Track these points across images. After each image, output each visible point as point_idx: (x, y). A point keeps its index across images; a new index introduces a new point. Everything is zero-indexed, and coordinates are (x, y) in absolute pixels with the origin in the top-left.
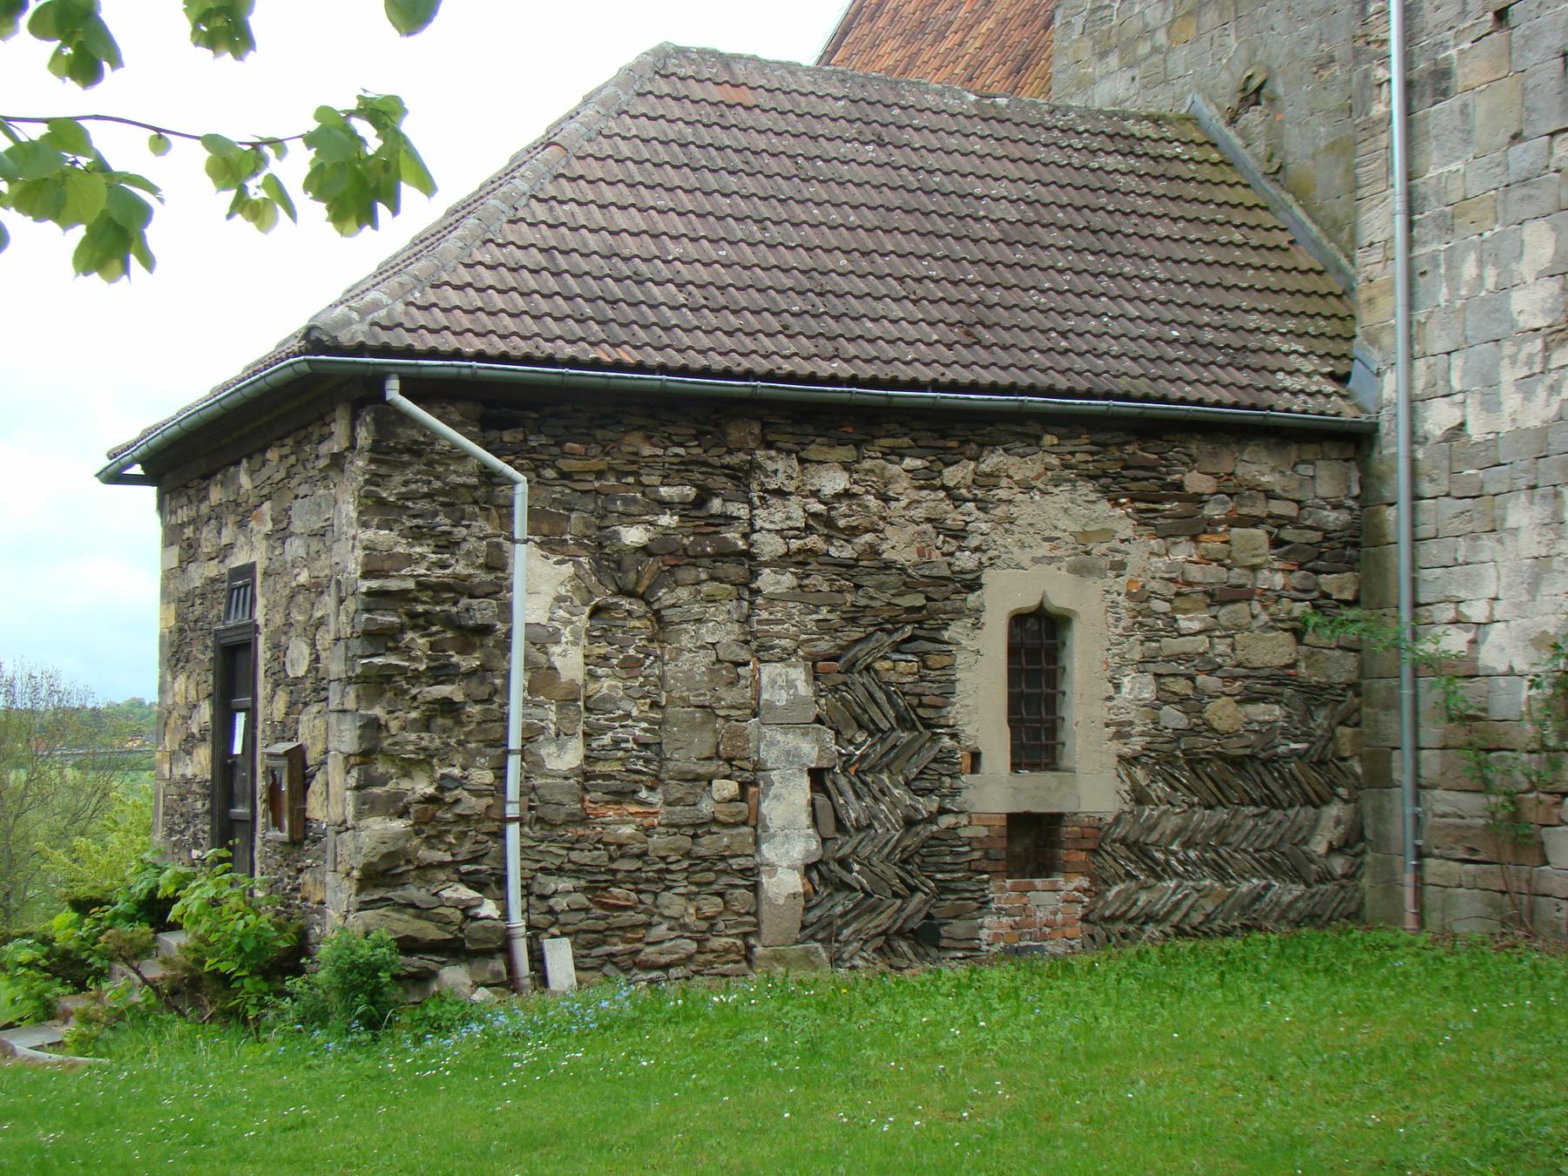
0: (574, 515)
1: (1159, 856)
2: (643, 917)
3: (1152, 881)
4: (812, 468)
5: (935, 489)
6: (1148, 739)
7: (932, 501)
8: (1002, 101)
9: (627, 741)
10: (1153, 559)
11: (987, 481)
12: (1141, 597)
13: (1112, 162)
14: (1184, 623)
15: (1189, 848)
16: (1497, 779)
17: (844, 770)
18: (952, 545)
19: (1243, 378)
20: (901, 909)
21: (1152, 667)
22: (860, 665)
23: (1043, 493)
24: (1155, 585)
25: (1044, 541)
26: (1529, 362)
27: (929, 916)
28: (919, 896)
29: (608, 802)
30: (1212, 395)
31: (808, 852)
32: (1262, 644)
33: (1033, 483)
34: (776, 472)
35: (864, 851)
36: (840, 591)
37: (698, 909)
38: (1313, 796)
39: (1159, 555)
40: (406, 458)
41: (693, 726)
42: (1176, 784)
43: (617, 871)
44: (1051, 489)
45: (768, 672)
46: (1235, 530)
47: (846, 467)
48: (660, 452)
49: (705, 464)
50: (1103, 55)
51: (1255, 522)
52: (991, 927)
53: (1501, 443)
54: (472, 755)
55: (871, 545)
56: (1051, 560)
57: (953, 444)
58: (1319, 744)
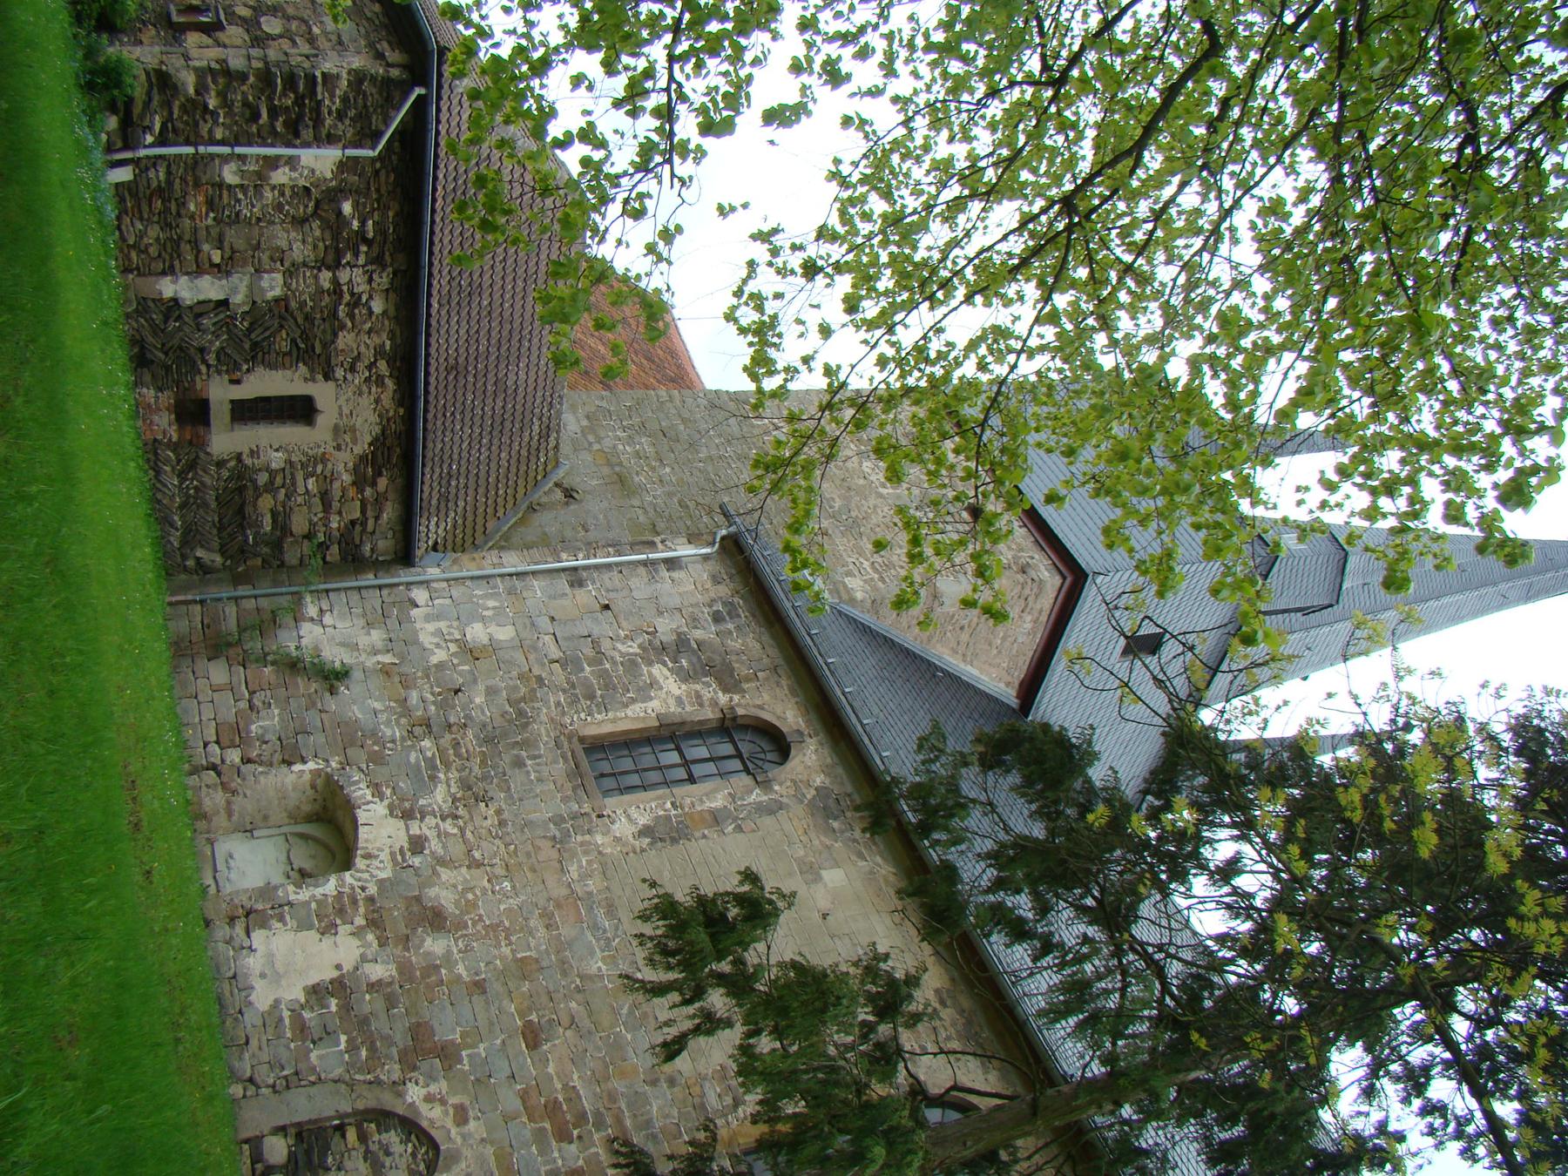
7: (369, 355)
10: (343, 464)
11: (380, 381)
12: (324, 459)
13: (536, 428)
14: (311, 481)
16: (246, 635)
19: (434, 502)
24: (330, 466)
25: (349, 411)
27: (152, 362)
30: (426, 488)
45: (279, 277)
47: (385, 312)
50: (588, 417)
51: (363, 512)
52: (149, 393)
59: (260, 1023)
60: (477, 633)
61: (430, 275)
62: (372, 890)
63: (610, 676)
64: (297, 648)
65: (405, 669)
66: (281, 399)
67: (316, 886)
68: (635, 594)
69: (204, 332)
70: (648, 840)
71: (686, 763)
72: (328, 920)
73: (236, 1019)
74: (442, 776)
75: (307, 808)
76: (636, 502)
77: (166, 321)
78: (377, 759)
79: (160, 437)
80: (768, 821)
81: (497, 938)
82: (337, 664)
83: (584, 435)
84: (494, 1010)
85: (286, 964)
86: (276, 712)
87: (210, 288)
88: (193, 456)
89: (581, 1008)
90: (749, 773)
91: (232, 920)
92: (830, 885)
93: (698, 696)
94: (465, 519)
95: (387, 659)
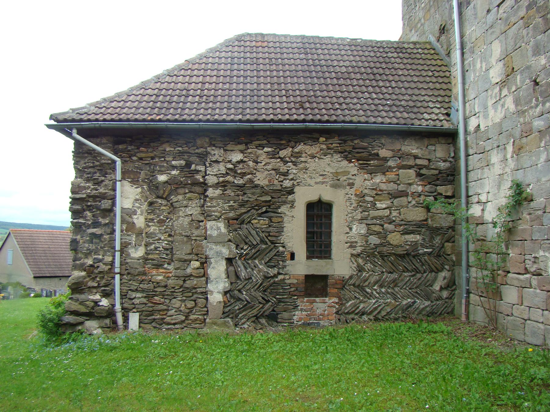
0: (142, 172)
1: (368, 290)
2: (165, 307)
3: (366, 299)
4: (228, 153)
5: (277, 158)
6: (363, 248)
7: (275, 163)
9: (160, 248)
10: (363, 182)
11: (298, 155)
14: (379, 205)
15: (382, 288)
17: (240, 259)
20: (262, 308)
22: (246, 222)
23: (319, 158)
24: (366, 191)
25: (318, 176)
26: (496, 97)
28: (270, 303)
29: (153, 268)
31: (225, 288)
32: (411, 213)
33: (315, 155)
34: (215, 154)
36: (238, 196)
37: (185, 305)
38: (434, 269)
39: (369, 180)
40: (86, 155)
41: (183, 243)
42: (376, 264)
43: (156, 291)
44: (322, 157)
45: (209, 224)
46: (401, 170)
47: (242, 152)
48: (172, 149)
51: (410, 167)
52: (297, 315)
53: (489, 130)
54: (105, 252)
56: (323, 183)
58: (437, 250)
60: (496, 73)
65: (517, 134)
79: (334, 310)
86: (541, 253)
87: (218, 271)
95: (510, 148)
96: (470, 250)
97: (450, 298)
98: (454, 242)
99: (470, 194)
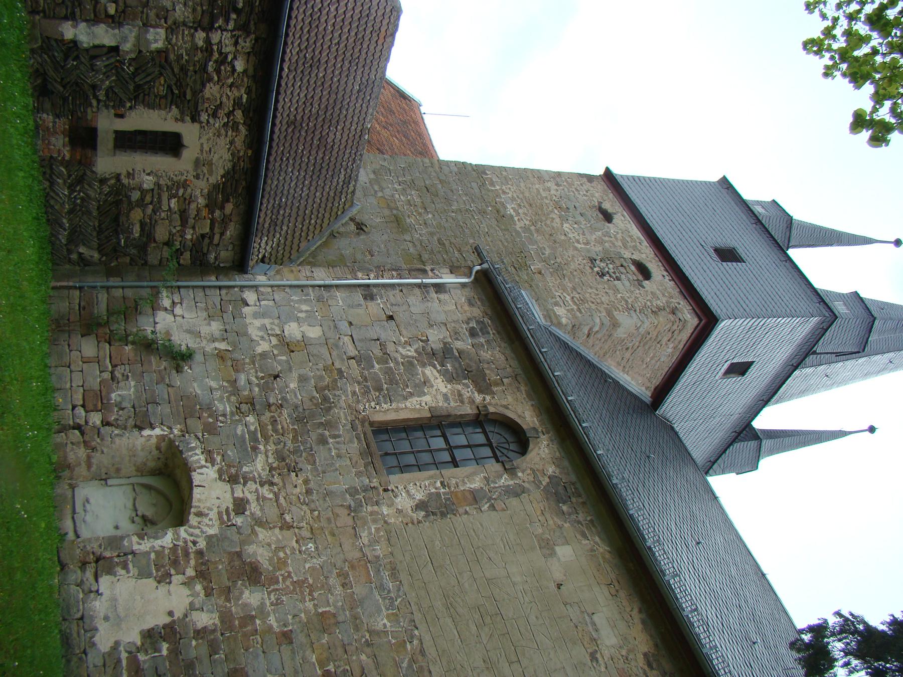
4: (245, 57)
5: (234, 106)
7: (229, 105)
8: (366, 137)
10: (199, 190)
11: (235, 127)
12: (185, 185)
13: (342, 176)
14: (173, 201)
16: (113, 319)
17: (118, 61)
18: (210, 112)
19: (266, 225)
20: (56, 81)
21: (156, 188)
22: (163, 71)
23: (229, 149)
24: (189, 190)
25: (207, 148)
27: (53, 93)
28: (61, 89)
30: (262, 215)
31: (82, 43)
35: (82, 67)
36: (195, 65)
45: (162, 32)
47: (245, 71)
49: (251, 13)
50: (374, 172)
51: (212, 228)
52: (48, 119)
55: (213, 79)
56: (202, 151)
57: (251, 115)
59: (101, 663)
60: (293, 330)
61: (286, 43)
62: (202, 544)
63: (393, 373)
64: (153, 332)
65: (236, 355)
66: (155, 134)
67: (156, 538)
68: (412, 309)
69: (97, 72)
70: (423, 513)
71: (450, 449)
72: (163, 569)
73: (80, 659)
74: (261, 447)
75: (151, 464)
76: (408, 238)
77: (66, 59)
78: (211, 429)
79: (55, 155)
80: (514, 502)
81: (302, 593)
82: (184, 348)
83: (371, 185)
84: (298, 659)
85: (129, 607)
86: (133, 383)
87: (104, 35)
88: (81, 173)
89: (370, 661)
90: (498, 461)
91: (84, 565)
92: (562, 559)
93: (460, 395)
94: (286, 239)
95: (223, 346)
96: (125, 290)
97: (70, 261)
98: (131, 264)
99: (182, 290)
